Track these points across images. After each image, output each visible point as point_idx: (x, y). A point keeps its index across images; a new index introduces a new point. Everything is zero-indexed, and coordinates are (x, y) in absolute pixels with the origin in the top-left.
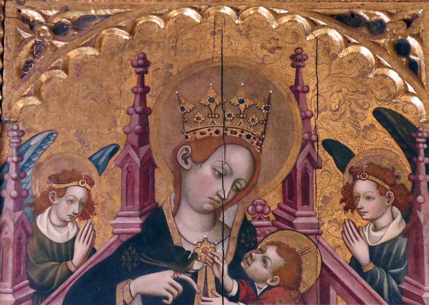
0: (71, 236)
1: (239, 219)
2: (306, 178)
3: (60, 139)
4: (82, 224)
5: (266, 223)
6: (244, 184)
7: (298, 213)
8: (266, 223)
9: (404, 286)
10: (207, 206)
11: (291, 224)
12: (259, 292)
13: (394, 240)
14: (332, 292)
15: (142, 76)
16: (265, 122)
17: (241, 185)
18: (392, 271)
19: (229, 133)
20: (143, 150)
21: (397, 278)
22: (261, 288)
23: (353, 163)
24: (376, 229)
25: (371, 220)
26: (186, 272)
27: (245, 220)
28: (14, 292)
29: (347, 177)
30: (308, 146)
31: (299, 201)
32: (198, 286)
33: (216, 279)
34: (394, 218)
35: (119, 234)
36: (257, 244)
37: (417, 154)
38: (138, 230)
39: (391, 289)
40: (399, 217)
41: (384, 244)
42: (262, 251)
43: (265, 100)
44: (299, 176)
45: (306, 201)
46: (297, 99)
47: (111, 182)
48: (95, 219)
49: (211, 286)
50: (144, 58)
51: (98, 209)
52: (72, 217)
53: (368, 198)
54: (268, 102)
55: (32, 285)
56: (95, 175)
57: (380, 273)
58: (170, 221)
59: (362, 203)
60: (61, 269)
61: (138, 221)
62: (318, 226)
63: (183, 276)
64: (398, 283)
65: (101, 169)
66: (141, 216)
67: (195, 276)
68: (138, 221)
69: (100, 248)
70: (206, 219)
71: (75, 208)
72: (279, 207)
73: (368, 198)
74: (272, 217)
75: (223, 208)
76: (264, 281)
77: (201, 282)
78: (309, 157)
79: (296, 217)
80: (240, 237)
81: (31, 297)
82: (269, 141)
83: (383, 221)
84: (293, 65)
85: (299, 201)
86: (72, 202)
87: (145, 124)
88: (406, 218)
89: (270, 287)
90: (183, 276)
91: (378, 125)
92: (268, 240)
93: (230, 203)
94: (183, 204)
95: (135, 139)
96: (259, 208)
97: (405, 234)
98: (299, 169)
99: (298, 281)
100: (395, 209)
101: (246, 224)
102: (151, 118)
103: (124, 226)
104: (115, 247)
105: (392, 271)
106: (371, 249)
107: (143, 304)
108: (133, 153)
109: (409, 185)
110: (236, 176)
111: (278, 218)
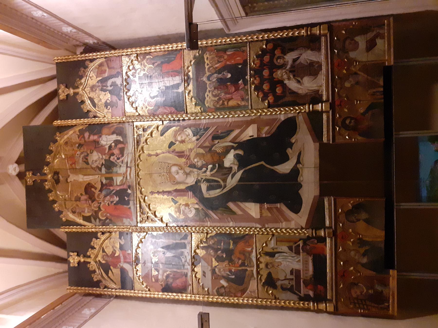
0: (193, 208)
1: (188, 168)
2: (177, 152)
3: (171, 212)
4: (191, 206)
5: (189, 162)
6: (180, 167)
7: (186, 154)
8: (189, 162)
9: (202, 128)
10: (185, 176)
11: (188, 156)
12: (205, 163)
13: (191, 130)
14: (204, 145)
15: (154, 193)
16: (165, 163)
17: (309, 108)
18: (199, 131)
19: (168, 171)
20: (173, 192)
21: (201, 129)
22: (204, 163)
23: (174, 141)
24: (189, 135)
25: (187, 136)
26: (201, 180)
27: (188, 167)
28: (207, 222)
29: (177, 143)
30: (170, 152)
31: (183, 154)
32: (204, 178)
33: (203, 173)
34: (186, 131)
35: (193, 197)
36: (194, 164)
37: (171, 126)
38: (192, 192)
39: (203, 131)
40: (186, 129)
41: (193, 133)
42: (195, 162)
43: (355, 292)
44: (178, 154)
45: (183, 152)
46: (159, 155)
47: (180, 199)
48: (189, 203)
49: (204, 174)
50: (150, 192)
51: (187, 202)
52: (189, 208)
53: (182, 137)
54: (160, 162)
55: (205, 218)
56: (178, 203)
57: (200, 134)
58: (189, 185)
59: (183, 139)
60: (201, 211)
61: (189, 192)
62: (189, 149)
63: (202, 181)
64: (201, 129)
65: (177, 202)
66: (188, 192)
67: (202, 179)
68: (189, 192)
69: (196, 202)
70: (188, 176)
71: (187, 208)
72: (185, 158)
73: (182, 137)
74: (187, 160)
75: (186, 172)
76: (203, 162)
77: (203, 177)
78: (173, 152)
79: (187, 155)
80: (192, 168)
81: (208, 218)
82: (169, 162)
83: (187, 134)
84: (151, 156)
85: (183, 154)
86: (185, 209)
87: (166, 192)
88: (186, 128)
89: (204, 160)
90: (202, 181)
91: (164, 135)
92: (193, 161)
93: (184, 170)
94: (185, 182)
95: (170, 194)
96: (185, 163)
97: (190, 128)
98: (176, 154)
99: (203, 154)
100: (184, 130)
101: (189, 167)
102: (165, 190)
103: (191, 196)
104: (196, 198)
105: (199, 131)
106: (194, 136)
107: (436, 313)
108: (173, 194)
109: (178, 127)
110: (178, 169)
111: (187, 159)
